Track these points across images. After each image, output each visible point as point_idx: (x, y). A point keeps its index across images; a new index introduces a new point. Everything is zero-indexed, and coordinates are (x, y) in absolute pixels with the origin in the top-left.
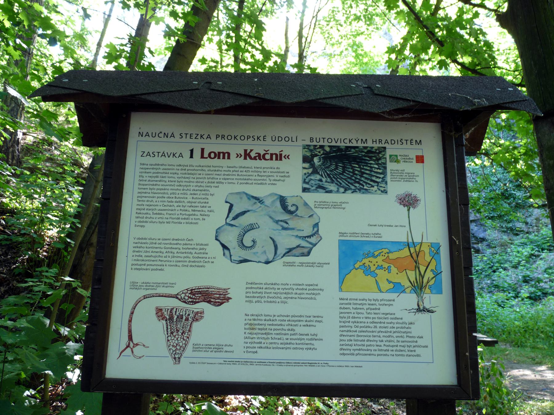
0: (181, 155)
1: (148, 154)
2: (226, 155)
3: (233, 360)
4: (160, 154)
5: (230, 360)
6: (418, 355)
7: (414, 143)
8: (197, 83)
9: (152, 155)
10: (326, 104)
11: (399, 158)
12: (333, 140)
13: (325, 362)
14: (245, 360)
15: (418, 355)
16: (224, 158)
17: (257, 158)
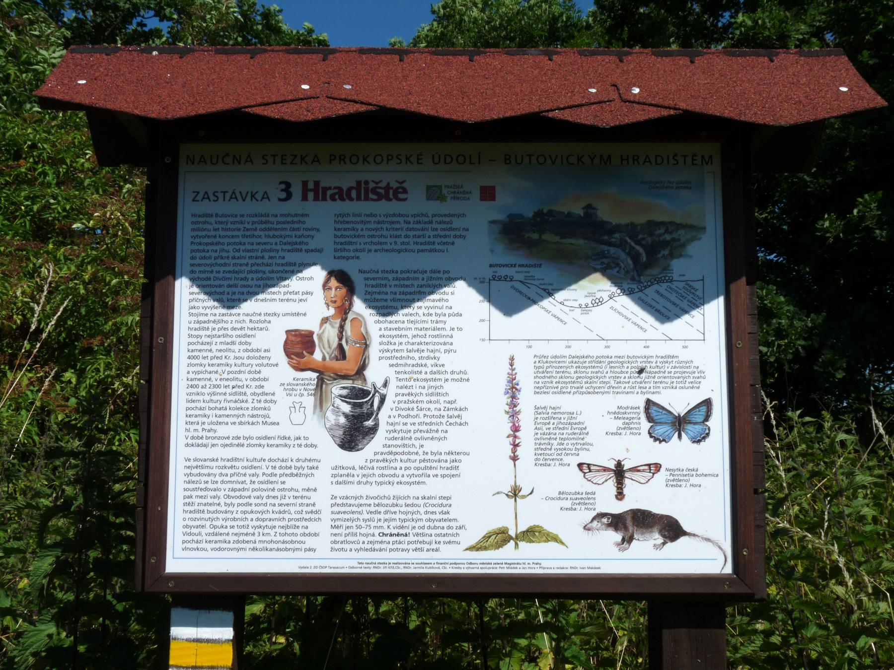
1: (206, 196)
3: (374, 561)
4: (228, 196)
5: (370, 561)
7: (699, 162)
8: (84, 82)
9: (212, 198)
10: (248, 113)
11: (445, 191)
13: (536, 562)
14: (395, 561)
17: (337, 197)
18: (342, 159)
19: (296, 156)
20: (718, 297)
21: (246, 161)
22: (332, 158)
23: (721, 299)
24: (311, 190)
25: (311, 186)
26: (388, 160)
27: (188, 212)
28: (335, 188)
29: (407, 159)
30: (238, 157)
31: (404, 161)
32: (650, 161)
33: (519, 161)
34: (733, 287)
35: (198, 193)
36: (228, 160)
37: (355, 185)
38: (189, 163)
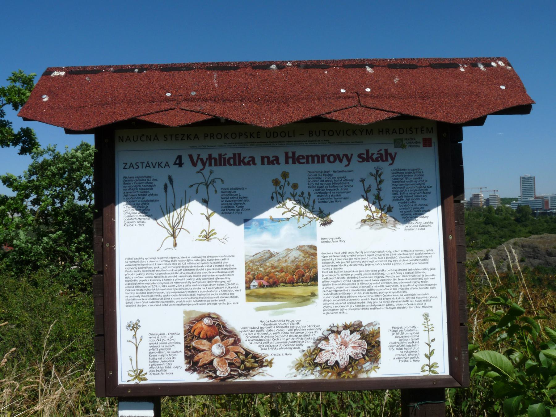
0: (167, 165)
1: (131, 166)
2: (316, 158)
4: (144, 165)
6: (237, 297)
15: (237, 297)
16: (313, 162)
17: (275, 162)
18: (212, 136)
19: (184, 135)
20: (437, 206)
21: (127, 140)
22: (206, 136)
23: (440, 208)
25: (290, 155)
26: (239, 136)
27: (122, 174)
29: (251, 135)
30: (149, 136)
31: (249, 137)
32: (396, 132)
34: (445, 201)
35: (126, 164)
36: (144, 138)
37: (232, 156)
38: (148, 140)
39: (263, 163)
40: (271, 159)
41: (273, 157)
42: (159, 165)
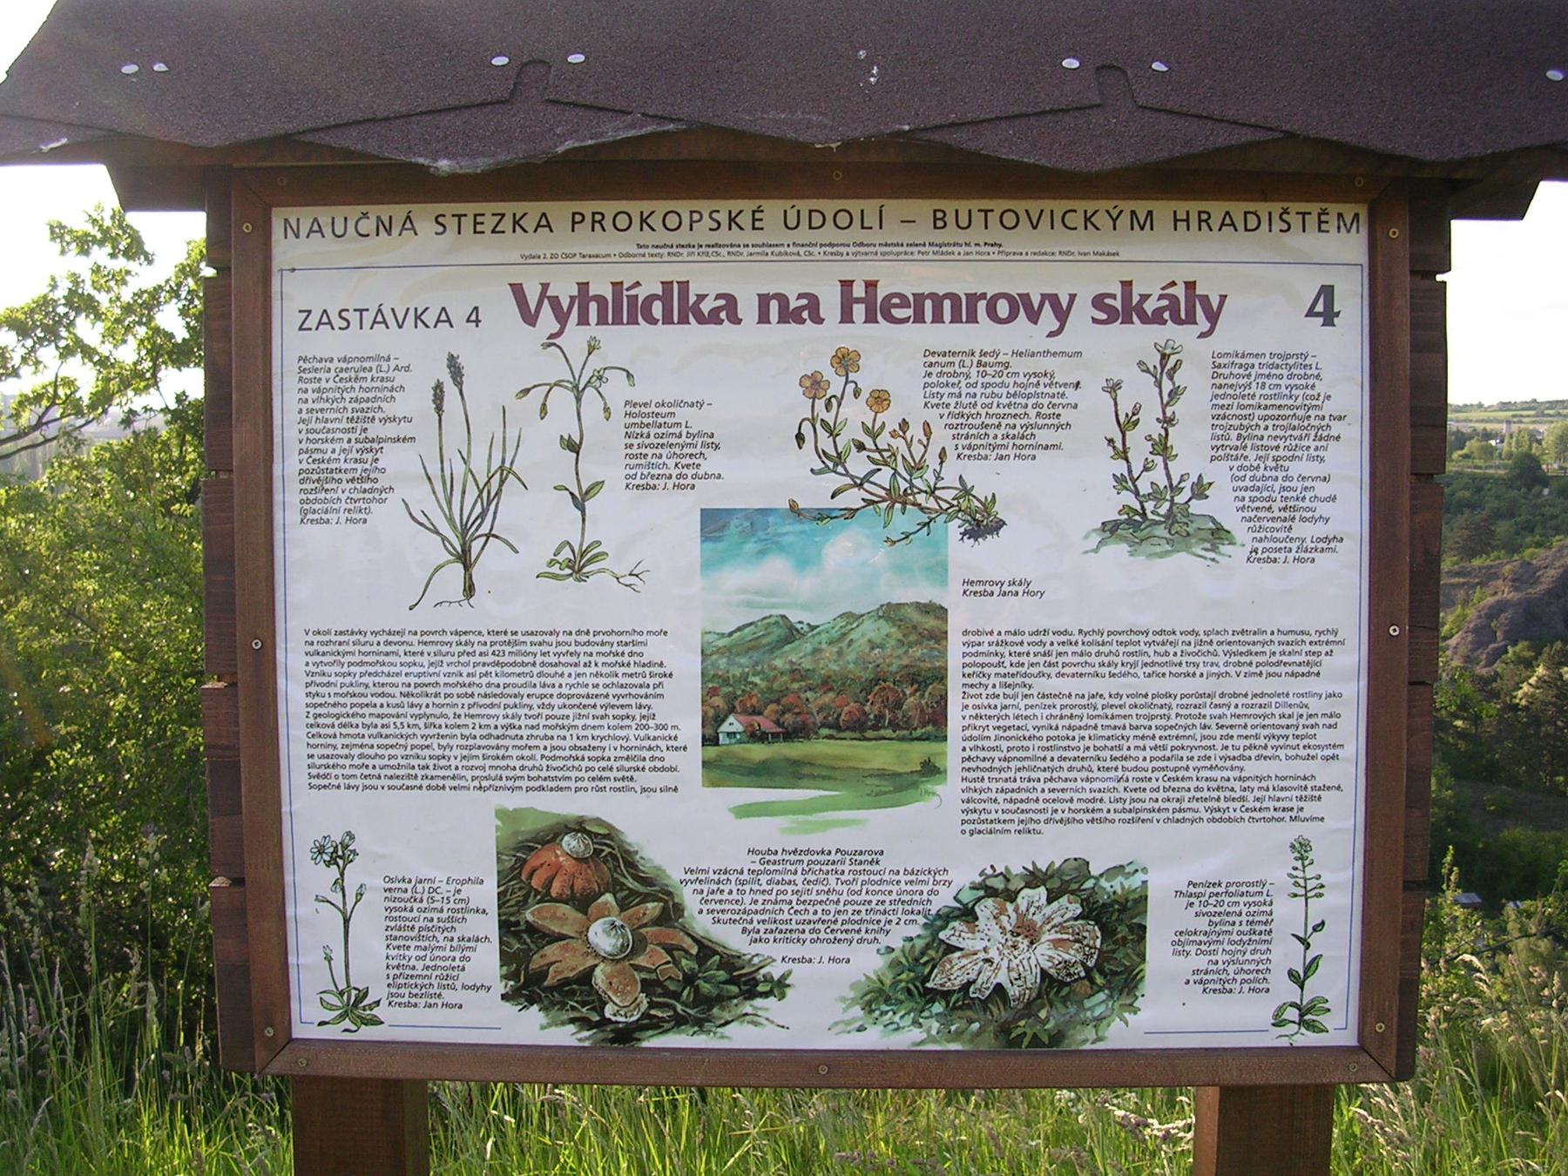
1: (325, 320)
2: (947, 304)
4: (368, 318)
8: (572, 59)
9: (338, 323)
12: (1023, 216)
16: (938, 318)
17: (805, 314)
24: (858, 300)
25: (859, 291)
28: (718, 297)
33: (964, 222)
39: (764, 318)
40: (793, 304)
41: (800, 296)
42: (418, 317)
